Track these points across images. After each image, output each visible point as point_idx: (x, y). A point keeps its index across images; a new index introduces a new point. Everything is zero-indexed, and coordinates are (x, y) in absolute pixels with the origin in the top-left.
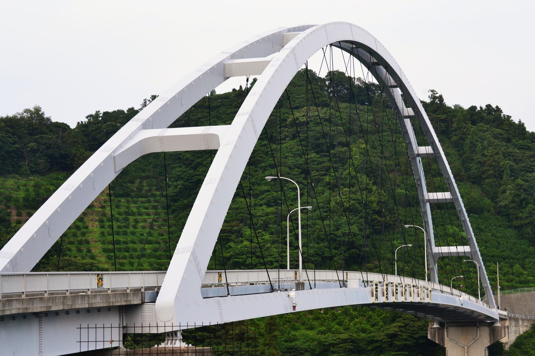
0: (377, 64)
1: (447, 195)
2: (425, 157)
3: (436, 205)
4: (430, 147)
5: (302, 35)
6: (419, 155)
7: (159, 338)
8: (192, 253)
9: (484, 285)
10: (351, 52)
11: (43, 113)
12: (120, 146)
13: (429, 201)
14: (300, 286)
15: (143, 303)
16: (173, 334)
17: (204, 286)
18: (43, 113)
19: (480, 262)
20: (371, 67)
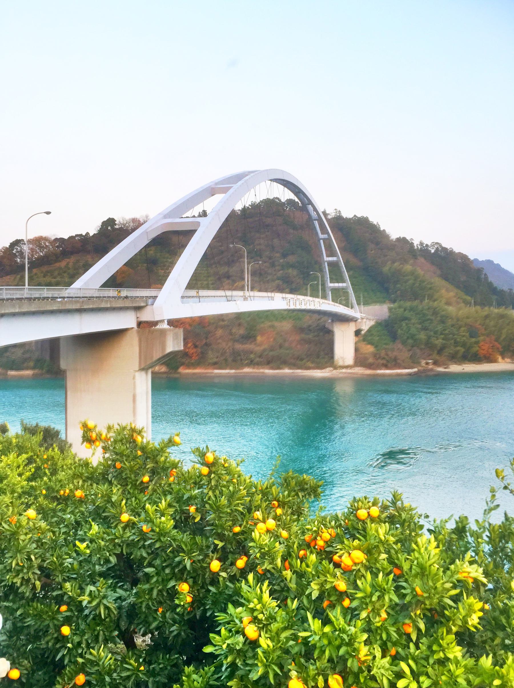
0: (299, 192)
1: (335, 259)
2: (324, 240)
3: (330, 264)
4: (326, 235)
5: (252, 174)
6: (321, 239)
7: (156, 323)
8: (41, 266)
9: (353, 302)
10: (285, 186)
11: (421, 244)
12: (151, 226)
13: (326, 261)
14: (245, 299)
15: (147, 305)
16: (162, 321)
17: (183, 297)
18: (421, 244)
19: (351, 291)
20: (296, 194)
